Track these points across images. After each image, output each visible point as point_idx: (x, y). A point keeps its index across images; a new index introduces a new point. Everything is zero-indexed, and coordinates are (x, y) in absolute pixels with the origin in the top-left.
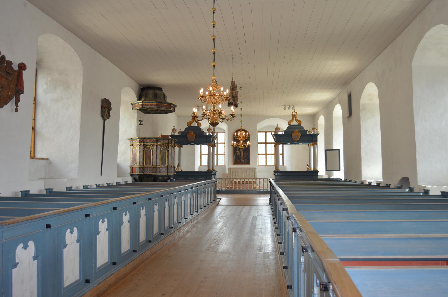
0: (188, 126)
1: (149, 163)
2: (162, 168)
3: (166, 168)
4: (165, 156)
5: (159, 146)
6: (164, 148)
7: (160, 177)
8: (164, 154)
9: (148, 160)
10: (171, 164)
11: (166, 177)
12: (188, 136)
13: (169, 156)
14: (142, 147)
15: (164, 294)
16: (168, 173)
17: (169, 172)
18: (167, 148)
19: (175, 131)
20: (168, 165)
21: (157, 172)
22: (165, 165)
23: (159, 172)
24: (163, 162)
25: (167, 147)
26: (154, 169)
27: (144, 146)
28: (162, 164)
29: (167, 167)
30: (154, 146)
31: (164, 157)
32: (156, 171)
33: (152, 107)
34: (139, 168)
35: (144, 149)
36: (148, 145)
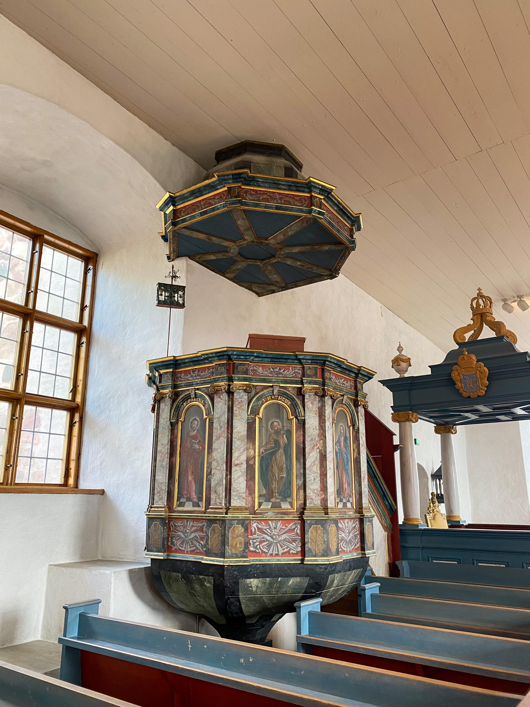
0: (458, 343)
1: (194, 496)
2: (263, 526)
3: (291, 526)
4: (281, 451)
5: (241, 397)
6: (278, 404)
7: (254, 582)
8: (277, 442)
9: (190, 478)
10: (325, 501)
11: (292, 581)
12: (455, 375)
14: (165, 407)
16: (303, 553)
17: (308, 546)
18: (294, 406)
19: (404, 365)
20: (305, 503)
21: (229, 550)
22: (285, 506)
23: (240, 548)
24: (274, 485)
25: (292, 400)
26: (214, 530)
27: (175, 404)
28: (268, 500)
29: (296, 516)
30: (216, 399)
31: (280, 456)
32: (224, 542)
33: (213, 210)
34: (150, 520)
35: (178, 417)
36: (193, 396)
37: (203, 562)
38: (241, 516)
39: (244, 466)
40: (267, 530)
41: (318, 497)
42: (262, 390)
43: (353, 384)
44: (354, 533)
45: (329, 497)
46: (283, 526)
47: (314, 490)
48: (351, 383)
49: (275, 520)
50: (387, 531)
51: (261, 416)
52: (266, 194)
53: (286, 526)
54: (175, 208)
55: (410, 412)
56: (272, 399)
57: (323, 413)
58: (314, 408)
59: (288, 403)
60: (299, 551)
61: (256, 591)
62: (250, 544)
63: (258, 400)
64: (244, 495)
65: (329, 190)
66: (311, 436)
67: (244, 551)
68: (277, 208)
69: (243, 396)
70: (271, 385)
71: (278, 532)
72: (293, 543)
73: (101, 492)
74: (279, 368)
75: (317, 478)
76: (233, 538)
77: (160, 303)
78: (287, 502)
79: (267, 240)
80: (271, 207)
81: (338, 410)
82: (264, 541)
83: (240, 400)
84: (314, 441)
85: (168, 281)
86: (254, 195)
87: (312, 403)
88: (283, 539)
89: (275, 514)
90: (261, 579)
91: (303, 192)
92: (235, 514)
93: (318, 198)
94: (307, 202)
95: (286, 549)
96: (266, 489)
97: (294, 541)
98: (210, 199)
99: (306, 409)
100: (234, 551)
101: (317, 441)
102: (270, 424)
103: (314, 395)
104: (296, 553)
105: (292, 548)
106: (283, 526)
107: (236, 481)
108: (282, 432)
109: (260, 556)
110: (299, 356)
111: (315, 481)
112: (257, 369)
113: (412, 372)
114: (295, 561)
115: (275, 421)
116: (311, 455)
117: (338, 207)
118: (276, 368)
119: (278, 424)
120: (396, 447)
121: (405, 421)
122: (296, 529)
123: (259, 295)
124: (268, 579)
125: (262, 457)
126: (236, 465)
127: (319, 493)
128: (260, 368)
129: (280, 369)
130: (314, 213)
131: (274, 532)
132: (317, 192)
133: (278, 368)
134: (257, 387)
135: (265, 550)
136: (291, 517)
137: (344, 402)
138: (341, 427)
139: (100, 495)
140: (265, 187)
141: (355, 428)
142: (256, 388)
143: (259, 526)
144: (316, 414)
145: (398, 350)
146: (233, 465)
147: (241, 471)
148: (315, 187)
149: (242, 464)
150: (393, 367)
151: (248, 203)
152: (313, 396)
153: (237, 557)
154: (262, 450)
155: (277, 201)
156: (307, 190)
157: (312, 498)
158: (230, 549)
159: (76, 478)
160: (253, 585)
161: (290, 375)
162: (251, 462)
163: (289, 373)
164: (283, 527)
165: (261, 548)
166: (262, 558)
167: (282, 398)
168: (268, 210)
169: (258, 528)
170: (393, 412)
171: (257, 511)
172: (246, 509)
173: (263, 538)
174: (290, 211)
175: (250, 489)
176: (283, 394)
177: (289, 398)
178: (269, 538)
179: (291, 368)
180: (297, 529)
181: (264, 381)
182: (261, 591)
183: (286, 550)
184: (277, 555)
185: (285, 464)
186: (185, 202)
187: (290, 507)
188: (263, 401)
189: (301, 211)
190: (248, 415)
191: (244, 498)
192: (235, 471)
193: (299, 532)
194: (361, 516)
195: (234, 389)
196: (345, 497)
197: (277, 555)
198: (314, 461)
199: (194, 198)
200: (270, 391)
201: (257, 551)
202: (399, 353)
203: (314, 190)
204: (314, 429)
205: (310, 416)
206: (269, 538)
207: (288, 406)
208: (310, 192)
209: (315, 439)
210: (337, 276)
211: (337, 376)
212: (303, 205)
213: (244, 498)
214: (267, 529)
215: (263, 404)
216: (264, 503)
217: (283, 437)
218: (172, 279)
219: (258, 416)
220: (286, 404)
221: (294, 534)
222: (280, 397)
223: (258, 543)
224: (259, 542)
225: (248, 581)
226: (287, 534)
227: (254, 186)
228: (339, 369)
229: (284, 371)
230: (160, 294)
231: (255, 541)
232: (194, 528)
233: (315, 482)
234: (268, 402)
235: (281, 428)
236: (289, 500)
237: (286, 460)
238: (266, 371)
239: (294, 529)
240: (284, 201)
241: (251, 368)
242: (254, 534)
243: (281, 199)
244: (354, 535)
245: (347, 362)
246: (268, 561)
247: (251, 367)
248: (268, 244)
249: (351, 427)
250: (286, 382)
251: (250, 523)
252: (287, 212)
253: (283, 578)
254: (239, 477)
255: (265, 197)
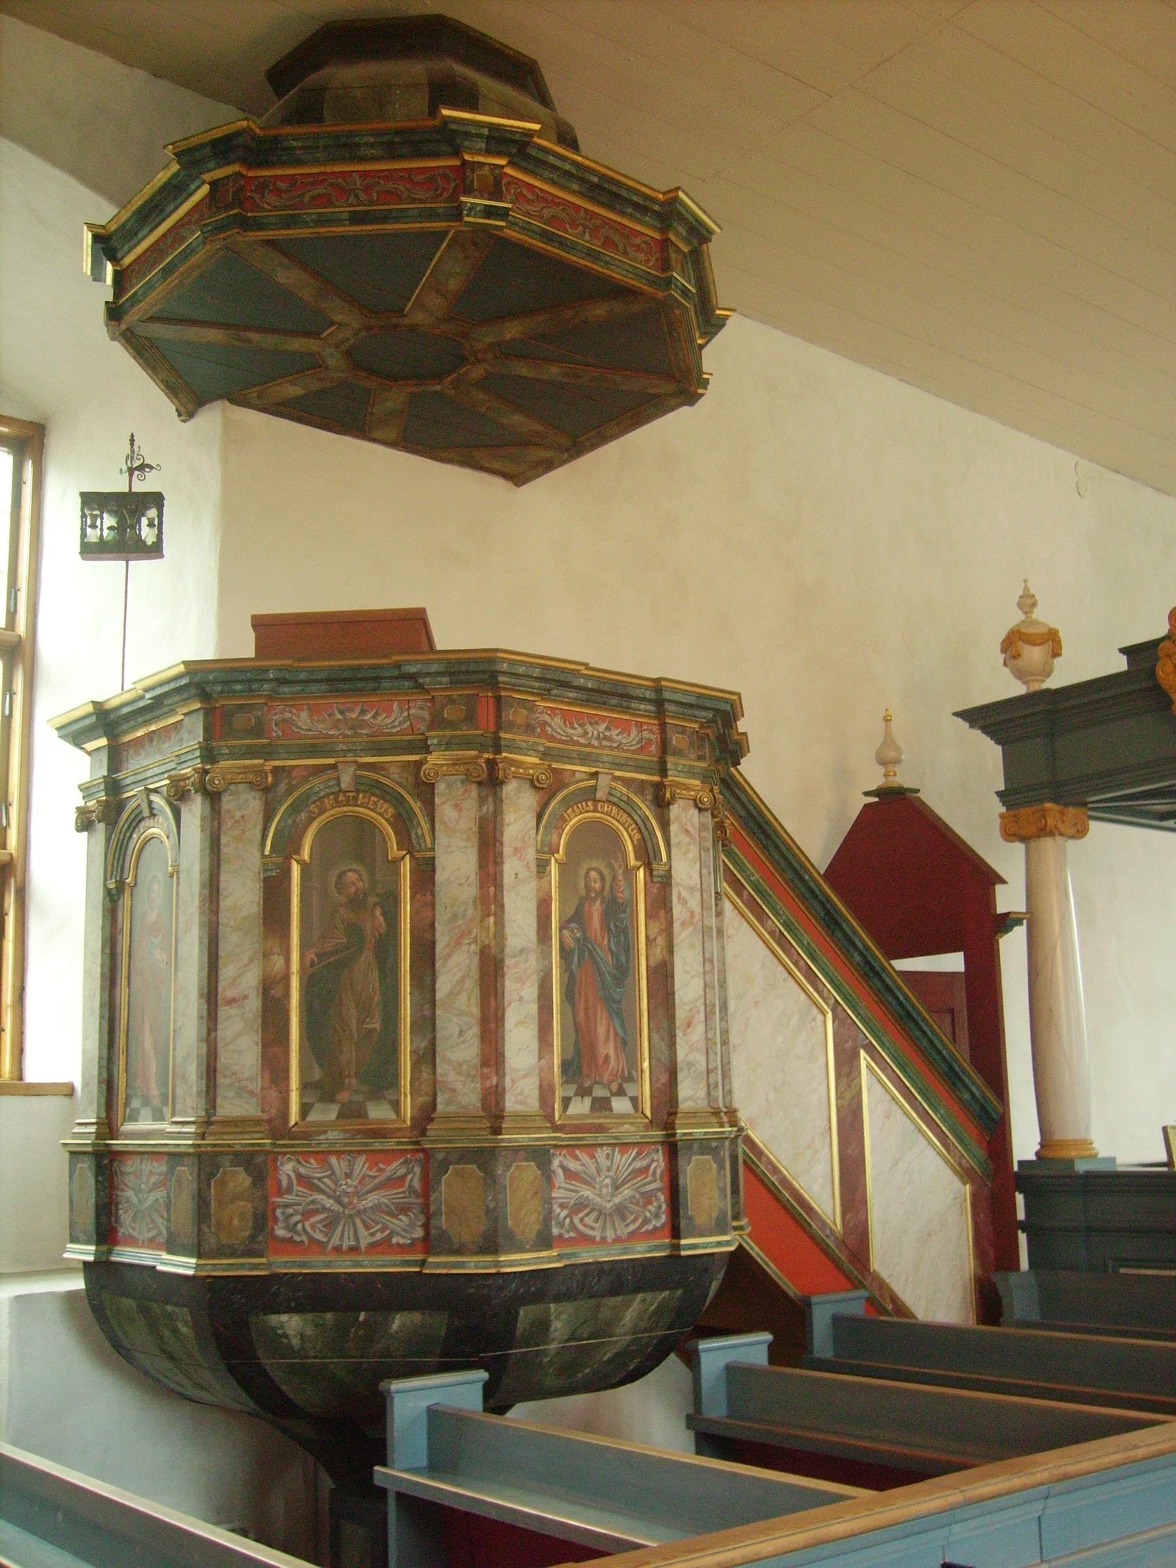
2: (311, 1169)
3: (395, 1167)
4: (367, 956)
6: (361, 822)
7: (291, 1324)
8: (354, 930)
11: (398, 1322)
13: (441, 946)
15: (516, 874)
18: (403, 824)
22: (378, 1112)
23: (241, 1230)
24: (348, 1055)
25: (400, 801)
28: (328, 1097)
31: (365, 966)
37: (160, 1268)
38: (239, 1142)
39: (254, 1004)
40: (325, 1180)
41: (472, 1085)
42: (306, 779)
43: (653, 737)
44: (640, 1187)
45: (513, 1081)
46: (370, 1168)
47: (460, 1065)
48: (646, 734)
49: (349, 1153)
50: (973, 1182)
51: (306, 854)
52: (324, 181)
53: (381, 1170)
54: (119, 268)
55: (1048, 805)
56: (338, 804)
57: (499, 837)
58: (461, 823)
59: (386, 811)
60: (418, 1239)
61: (302, 1348)
62: (276, 1220)
63: (295, 808)
64: (256, 1086)
65: (517, 137)
66: (452, 906)
67: (253, 1237)
68: (356, 218)
69: (247, 801)
70: (331, 761)
71: (355, 1187)
72: (402, 1217)
73: (66, 1091)
74: (359, 707)
75: (469, 1028)
76: (220, 1203)
77: (90, 550)
78: (627, 1098)
79: (404, 316)
80: (337, 221)
81: (574, 821)
82: (316, 1212)
83: (238, 814)
84: (460, 922)
85: (118, 484)
86: (286, 191)
87: (456, 806)
88: (370, 1204)
89: (348, 1135)
90: (310, 1316)
91: (437, 155)
92: (226, 1137)
93: (487, 167)
94: (453, 184)
95: (379, 1234)
96: (320, 1065)
97: (404, 1209)
98: (183, 225)
99: (437, 826)
100: (224, 1239)
101: (471, 920)
102: (334, 879)
103: (462, 782)
104: (411, 1246)
105: (398, 1230)
106: (370, 1168)
107: (231, 1047)
108: (371, 900)
109: (305, 1252)
110: (407, 667)
111: (462, 1039)
112: (294, 717)
113: (1064, 675)
114: (403, 1266)
115: (350, 870)
116: (453, 961)
117: (582, 180)
118: (351, 710)
119: (356, 877)
120: (1005, 922)
121: (1039, 836)
122: (410, 1176)
123: (518, 479)
124: (329, 1316)
125: (311, 977)
126: (231, 1002)
127: (473, 1072)
128: (304, 715)
129: (363, 712)
130: (467, 215)
131: (344, 1187)
132: (480, 149)
133: (358, 709)
134: (294, 774)
135: (319, 1236)
136: (391, 1144)
137: (600, 795)
138: (593, 874)
139: (62, 1097)
140: (317, 162)
141: (655, 873)
142: (290, 776)
143: (302, 1170)
144: (467, 840)
145: (1020, 605)
146: (220, 1002)
147: (242, 1018)
148: (467, 135)
149: (246, 997)
150: (1005, 664)
151: (266, 221)
152: (459, 784)
153: (233, 1254)
154: (311, 956)
155: (357, 196)
156: (444, 148)
157: (453, 1087)
158: (214, 1233)
159: (17, 1052)
160: (291, 1332)
161: (395, 727)
162: (277, 992)
163: (392, 719)
164: (372, 1173)
165: (308, 1228)
166: (309, 1258)
167: (369, 800)
168: (330, 229)
169: (300, 1176)
170: (1004, 809)
171: (293, 1129)
172: (258, 1122)
173: (313, 1202)
174: (397, 220)
175: (274, 1067)
176: (368, 786)
177: (389, 797)
178: (329, 1203)
179: (395, 705)
180: (412, 1179)
181: (313, 750)
182: (315, 1348)
183: (379, 1236)
184: (354, 1250)
185: (378, 993)
186: (135, 246)
187: (394, 1117)
188: (311, 812)
189: (432, 215)
190: (263, 856)
191: (252, 1094)
192: (227, 1019)
193: (417, 1184)
194: (668, 1136)
195: (217, 782)
196: (605, 1082)
197: (354, 1250)
198: (462, 981)
199: (151, 231)
200: (330, 780)
201: (298, 1239)
202: (1023, 617)
203: (467, 143)
204: (461, 885)
205: (449, 847)
206: (329, 1203)
207: (387, 820)
208: (456, 153)
209: (464, 915)
210: (700, 391)
211: (567, 717)
212: (441, 195)
213: (252, 1094)
214: (324, 1177)
215: (311, 820)
216: (317, 1106)
217: (373, 916)
218: (131, 475)
219: (294, 857)
220: (379, 816)
221: (404, 1192)
222: (361, 795)
223: (298, 1218)
224: (302, 1214)
225: (275, 1319)
226: (382, 1192)
227: (284, 164)
228: (571, 695)
229: (374, 717)
230: (89, 523)
231: (290, 1211)
232: (153, 1180)
233: (464, 1042)
234: (327, 814)
235: (366, 887)
236: (390, 1095)
237: (382, 979)
238: (323, 721)
239: (405, 1176)
240: (379, 193)
241: (275, 718)
242: (289, 1190)
243: (367, 189)
244: (642, 1194)
245: (587, 669)
246: (328, 1266)
247: (276, 714)
248: (414, 328)
249: (642, 870)
250: (380, 750)
251: (275, 1161)
252: (389, 226)
253: (372, 1313)
254: (238, 1035)
255: (320, 190)
